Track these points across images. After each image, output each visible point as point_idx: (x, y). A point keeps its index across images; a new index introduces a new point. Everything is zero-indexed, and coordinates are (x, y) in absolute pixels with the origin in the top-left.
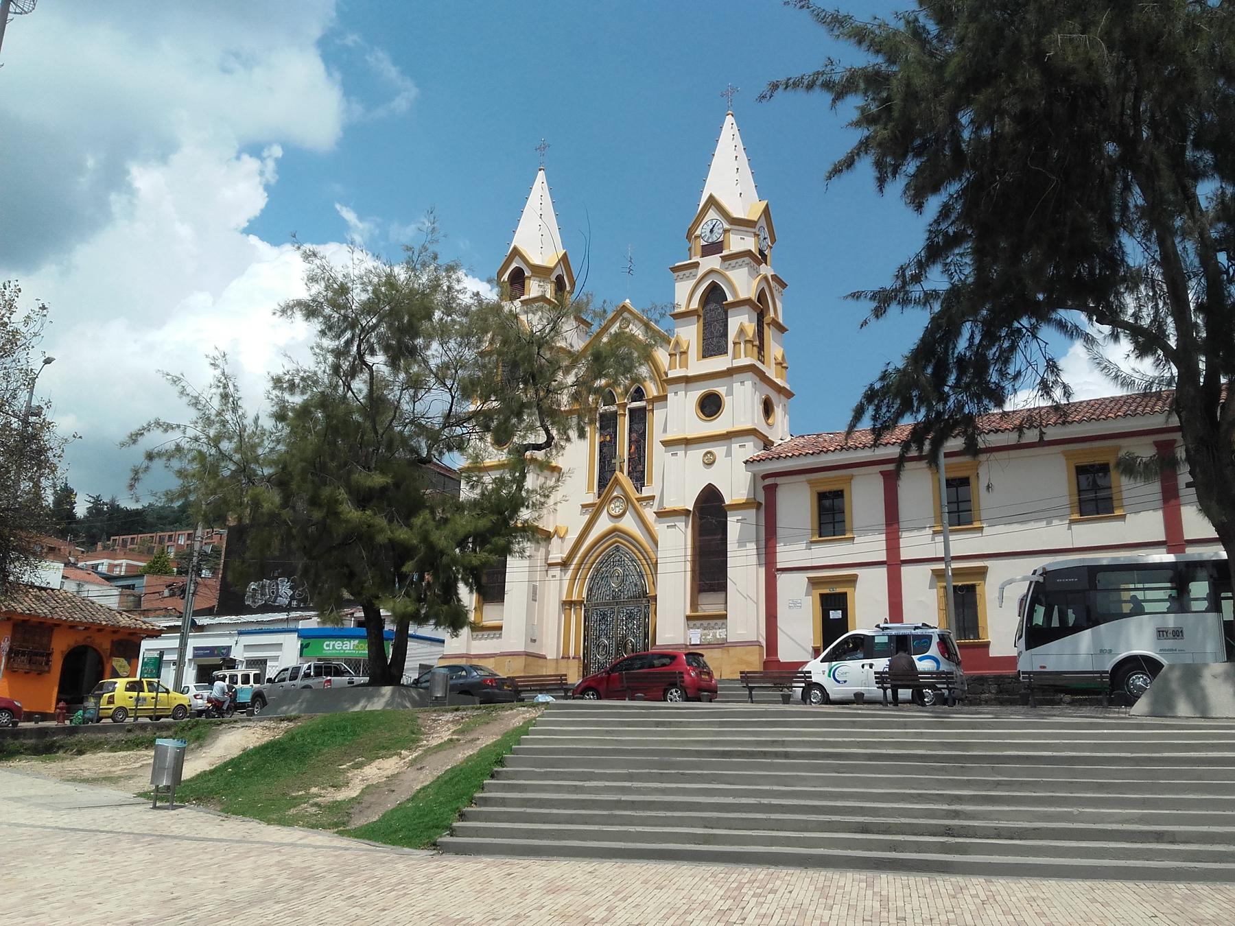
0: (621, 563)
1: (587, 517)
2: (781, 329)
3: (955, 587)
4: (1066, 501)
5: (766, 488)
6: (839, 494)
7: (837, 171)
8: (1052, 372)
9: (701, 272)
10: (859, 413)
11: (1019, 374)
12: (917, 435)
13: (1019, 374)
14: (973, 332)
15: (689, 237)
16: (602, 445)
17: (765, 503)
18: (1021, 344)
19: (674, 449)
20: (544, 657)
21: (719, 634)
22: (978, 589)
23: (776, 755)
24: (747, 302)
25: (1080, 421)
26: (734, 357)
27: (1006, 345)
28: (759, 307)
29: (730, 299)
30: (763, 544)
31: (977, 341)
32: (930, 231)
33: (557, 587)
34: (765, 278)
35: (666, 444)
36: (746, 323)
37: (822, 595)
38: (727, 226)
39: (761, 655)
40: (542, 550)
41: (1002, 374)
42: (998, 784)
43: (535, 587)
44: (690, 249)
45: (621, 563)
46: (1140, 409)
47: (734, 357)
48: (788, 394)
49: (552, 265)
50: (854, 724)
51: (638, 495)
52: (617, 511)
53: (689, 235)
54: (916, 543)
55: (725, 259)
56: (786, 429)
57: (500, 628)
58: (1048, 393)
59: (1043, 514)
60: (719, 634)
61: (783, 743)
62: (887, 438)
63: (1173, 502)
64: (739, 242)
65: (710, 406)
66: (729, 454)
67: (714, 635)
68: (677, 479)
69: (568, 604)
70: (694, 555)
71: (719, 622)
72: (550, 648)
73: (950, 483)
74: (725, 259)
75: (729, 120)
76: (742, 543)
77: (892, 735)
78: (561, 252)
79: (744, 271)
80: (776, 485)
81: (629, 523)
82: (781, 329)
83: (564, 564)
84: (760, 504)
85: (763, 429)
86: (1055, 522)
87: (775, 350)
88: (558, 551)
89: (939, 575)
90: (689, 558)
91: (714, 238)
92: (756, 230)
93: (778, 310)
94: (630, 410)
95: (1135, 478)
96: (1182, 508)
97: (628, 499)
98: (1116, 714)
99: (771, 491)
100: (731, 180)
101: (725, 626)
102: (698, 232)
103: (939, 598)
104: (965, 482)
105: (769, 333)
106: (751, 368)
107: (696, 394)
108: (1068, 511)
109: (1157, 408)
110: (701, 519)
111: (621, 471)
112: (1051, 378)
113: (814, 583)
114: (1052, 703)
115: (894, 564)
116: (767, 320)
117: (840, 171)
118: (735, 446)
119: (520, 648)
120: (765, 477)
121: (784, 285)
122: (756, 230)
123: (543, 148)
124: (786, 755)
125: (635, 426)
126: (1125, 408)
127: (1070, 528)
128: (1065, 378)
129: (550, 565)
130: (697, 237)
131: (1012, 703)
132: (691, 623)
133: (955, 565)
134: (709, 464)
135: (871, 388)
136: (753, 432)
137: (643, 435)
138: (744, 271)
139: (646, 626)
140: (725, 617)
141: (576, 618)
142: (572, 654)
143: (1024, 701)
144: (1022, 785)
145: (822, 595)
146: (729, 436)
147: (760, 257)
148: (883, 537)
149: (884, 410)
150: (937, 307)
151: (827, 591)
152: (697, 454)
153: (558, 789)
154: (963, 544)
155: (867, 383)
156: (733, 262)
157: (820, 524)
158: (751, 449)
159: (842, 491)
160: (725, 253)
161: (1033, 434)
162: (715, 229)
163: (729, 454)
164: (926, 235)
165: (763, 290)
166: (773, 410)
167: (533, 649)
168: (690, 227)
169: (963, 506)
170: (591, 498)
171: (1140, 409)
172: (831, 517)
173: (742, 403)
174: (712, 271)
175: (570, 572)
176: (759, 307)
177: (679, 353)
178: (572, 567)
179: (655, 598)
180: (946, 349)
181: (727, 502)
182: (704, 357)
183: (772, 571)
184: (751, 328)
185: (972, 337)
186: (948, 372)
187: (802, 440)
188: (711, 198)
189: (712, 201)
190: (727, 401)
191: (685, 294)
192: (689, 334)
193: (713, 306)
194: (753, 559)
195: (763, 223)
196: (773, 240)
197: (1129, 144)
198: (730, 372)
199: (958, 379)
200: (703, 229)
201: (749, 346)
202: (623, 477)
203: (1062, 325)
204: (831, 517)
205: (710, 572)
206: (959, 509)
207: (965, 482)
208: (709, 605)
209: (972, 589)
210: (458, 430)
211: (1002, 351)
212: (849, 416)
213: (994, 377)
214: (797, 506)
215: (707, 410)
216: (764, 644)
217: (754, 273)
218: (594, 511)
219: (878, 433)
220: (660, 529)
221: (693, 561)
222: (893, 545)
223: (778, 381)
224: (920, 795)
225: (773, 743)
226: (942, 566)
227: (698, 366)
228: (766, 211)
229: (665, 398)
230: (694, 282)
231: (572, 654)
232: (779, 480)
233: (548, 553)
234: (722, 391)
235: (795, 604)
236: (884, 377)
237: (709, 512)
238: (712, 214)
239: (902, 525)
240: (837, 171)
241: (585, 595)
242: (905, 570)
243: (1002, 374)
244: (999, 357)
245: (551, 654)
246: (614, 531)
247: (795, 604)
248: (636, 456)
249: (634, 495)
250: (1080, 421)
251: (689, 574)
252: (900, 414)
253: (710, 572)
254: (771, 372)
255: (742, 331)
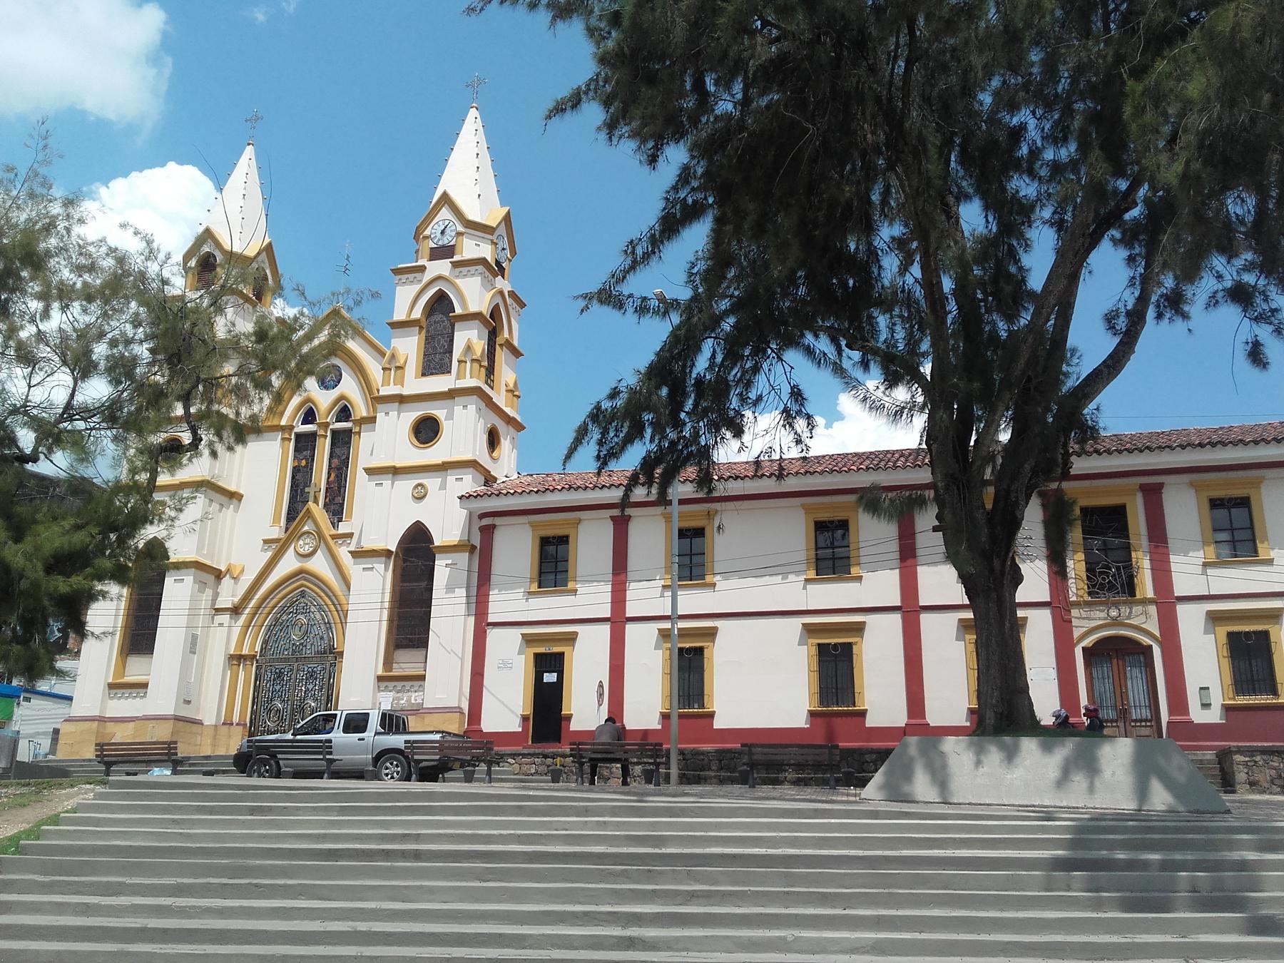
0: (306, 612)
1: (269, 554)
2: (516, 353)
3: (681, 650)
4: (802, 556)
5: (482, 529)
6: (564, 540)
7: (559, 109)
8: (796, 400)
9: (427, 277)
10: (582, 433)
11: (760, 398)
12: (648, 465)
13: (760, 398)
14: (714, 351)
15: (416, 237)
16: (296, 470)
17: (480, 549)
18: (765, 366)
19: (378, 479)
20: (200, 723)
21: (415, 698)
22: (706, 651)
23: (404, 855)
24: (477, 316)
25: (822, 472)
26: (458, 378)
27: (749, 365)
28: (492, 323)
29: (458, 310)
30: (474, 591)
31: (719, 359)
32: (667, 199)
33: (225, 637)
34: (501, 293)
35: (370, 471)
36: (475, 340)
37: (537, 656)
38: (460, 229)
39: (461, 723)
40: (209, 592)
41: (743, 399)
42: (692, 897)
43: (195, 637)
44: (417, 252)
45: (306, 612)
46: (883, 463)
47: (458, 378)
48: (519, 427)
49: (251, 252)
50: (520, 811)
51: (334, 532)
52: (307, 549)
53: (418, 235)
54: (646, 596)
55: (456, 265)
56: (513, 464)
57: (144, 686)
58: (791, 425)
59: (780, 569)
60: (415, 698)
61: (418, 838)
62: (613, 465)
63: (909, 562)
64: (472, 248)
65: (426, 430)
66: (443, 487)
67: (409, 700)
68: (380, 515)
69: (237, 659)
70: (393, 601)
71: (416, 684)
72: (209, 713)
73: (683, 533)
74: (456, 265)
75: (473, 113)
76: (450, 588)
77: (565, 826)
78: (267, 241)
79: (477, 280)
80: (494, 526)
81: (319, 565)
82: (516, 353)
83: (236, 611)
84: (473, 548)
85: (485, 460)
86: (792, 577)
87: (506, 373)
88: (229, 594)
89: (665, 635)
90: (387, 605)
91: (445, 241)
92: (494, 238)
93: (514, 330)
94: (334, 432)
95: (879, 516)
96: (919, 569)
97: (320, 536)
98: (845, 797)
99: (487, 532)
100: (469, 178)
101: (422, 688)
102: (427, 232)
103: (664, 660)
104: (699, 532)
105: (501, 355)
106: (476, 391)
107: (411, 415)
108: (803, 567)
109: (899, 464)
110: (405, 561)
111: (316, 501)
112: (795, 408)
113: (529, 640)
114: (775, 782)
115: (618, 621)
116: (499, 340)
117: (563, 110)
118: (451, 478)
119: (170, 711)
120: (482, 516)
121: (522, 305)
122: (494, 238)
123: (256, 118)
124: (417, 855)
125: (337, 450)
126: (868, 462)
127: (805, 588)
128: (809, 408)
129: (217, 610)
130: (426, 238)
131: (733, 781)
132: (383, 685)
133: (683, 624)
134: (420, 498)
135: (598, 407)
136: (473, 464)
137: (345, 463)
138: (477, 280)
139: (330, 687)
140: (422, 678)
141: (245, 675)
142: (236, 719)
143: (744, 780)
144: (725, 897)
145: (537, 656)
146: (444, 467)
147: (498, 269)
148: (609, 588)
149: (612, 434)
150: (676, 318)
151: (541, 650)
152: (406, 485)
153: (60, 908)
154: (693, 601)
155: (594, 401)
156: (464, 270)
157: (541, 573)
158: (468, 483)
159: (567, 537)
160: (456, 258)
161: (775, 483)
162: (448, 231)
163: (443, 487)
164: (661, 204)
165: (496, 307)
166: (499, 442)
167: (185, 712)
168: (422, 225)
169: (696, 559)
170: (277, 532)
171: (883, 463)
172: (553, 566)
173: (462, 432)
174: (439, 278)
175: (243, 617)
176: (492, 323)
177: (394, 367)
178: (247, 611)
179: (342, 653)
180: (684, 366)
181: (436, 544)
182: (424, 375)
183: (482, 626)
184: (480, 346)
185: (713, 356)
186: (685, 395)
187: (530, 478)
188: (445, 195)
189: (446, 199)
190: (446, 426)
191: (407, 301)
192: (409, 347)
193: (438, 317)
194: (462, 609)
195: (502, 230)
196: (514, 253)
197: (894, 121)
198: (452, 394)
199: (696, 405)
200: (433, 229)
201: (476, 365)
202: (317, 509)
203: (809, 351)
204: (553, 566)
205: (409, 625)
206: (691, 562)
207: (699, 532)
208: (406, 663)
209: (699, 651)
210: (80, 425)
211: (744, 372)
212: (570, 437)
213: (735, 403)
214: (516, 550)
215: (423, 436)
216: (466, 712)
217: (488, 285)
218: (279, 548)
219: (603, 461)
220: (354, 569)
221: (391, 609)
222: (619, 599)
223: (508, 410)
224: (586, 914)
225: (404, 838)
226: (667, 625)
227: (415, 384)
228: (507, 219)
229: (372, 420)
230: (418, 287)
231: (236, 719)
232: (498, 521)
233: (216, 595)
234: (440, 413)
235: (505, 665)
236: (614, 394)
237: (416, 552)
238: (445, 213)
239: (630, 575)
240: (559, 109)
241: (258, 648)
242: (630, 627)
243: (743, 399)
244: (741, 379)
245: (209, 718)
246: (300, 572)
247: (505, 665)
248: (335, 486)
249: (328, 530)
250: (822, 472)
251: (385, 625)
252: (629, 440)
253: (409, 625)
254: (500, 399)
255: (469, 348)
